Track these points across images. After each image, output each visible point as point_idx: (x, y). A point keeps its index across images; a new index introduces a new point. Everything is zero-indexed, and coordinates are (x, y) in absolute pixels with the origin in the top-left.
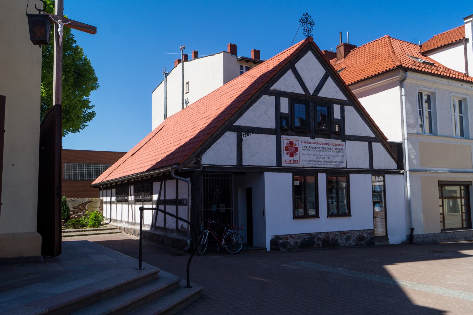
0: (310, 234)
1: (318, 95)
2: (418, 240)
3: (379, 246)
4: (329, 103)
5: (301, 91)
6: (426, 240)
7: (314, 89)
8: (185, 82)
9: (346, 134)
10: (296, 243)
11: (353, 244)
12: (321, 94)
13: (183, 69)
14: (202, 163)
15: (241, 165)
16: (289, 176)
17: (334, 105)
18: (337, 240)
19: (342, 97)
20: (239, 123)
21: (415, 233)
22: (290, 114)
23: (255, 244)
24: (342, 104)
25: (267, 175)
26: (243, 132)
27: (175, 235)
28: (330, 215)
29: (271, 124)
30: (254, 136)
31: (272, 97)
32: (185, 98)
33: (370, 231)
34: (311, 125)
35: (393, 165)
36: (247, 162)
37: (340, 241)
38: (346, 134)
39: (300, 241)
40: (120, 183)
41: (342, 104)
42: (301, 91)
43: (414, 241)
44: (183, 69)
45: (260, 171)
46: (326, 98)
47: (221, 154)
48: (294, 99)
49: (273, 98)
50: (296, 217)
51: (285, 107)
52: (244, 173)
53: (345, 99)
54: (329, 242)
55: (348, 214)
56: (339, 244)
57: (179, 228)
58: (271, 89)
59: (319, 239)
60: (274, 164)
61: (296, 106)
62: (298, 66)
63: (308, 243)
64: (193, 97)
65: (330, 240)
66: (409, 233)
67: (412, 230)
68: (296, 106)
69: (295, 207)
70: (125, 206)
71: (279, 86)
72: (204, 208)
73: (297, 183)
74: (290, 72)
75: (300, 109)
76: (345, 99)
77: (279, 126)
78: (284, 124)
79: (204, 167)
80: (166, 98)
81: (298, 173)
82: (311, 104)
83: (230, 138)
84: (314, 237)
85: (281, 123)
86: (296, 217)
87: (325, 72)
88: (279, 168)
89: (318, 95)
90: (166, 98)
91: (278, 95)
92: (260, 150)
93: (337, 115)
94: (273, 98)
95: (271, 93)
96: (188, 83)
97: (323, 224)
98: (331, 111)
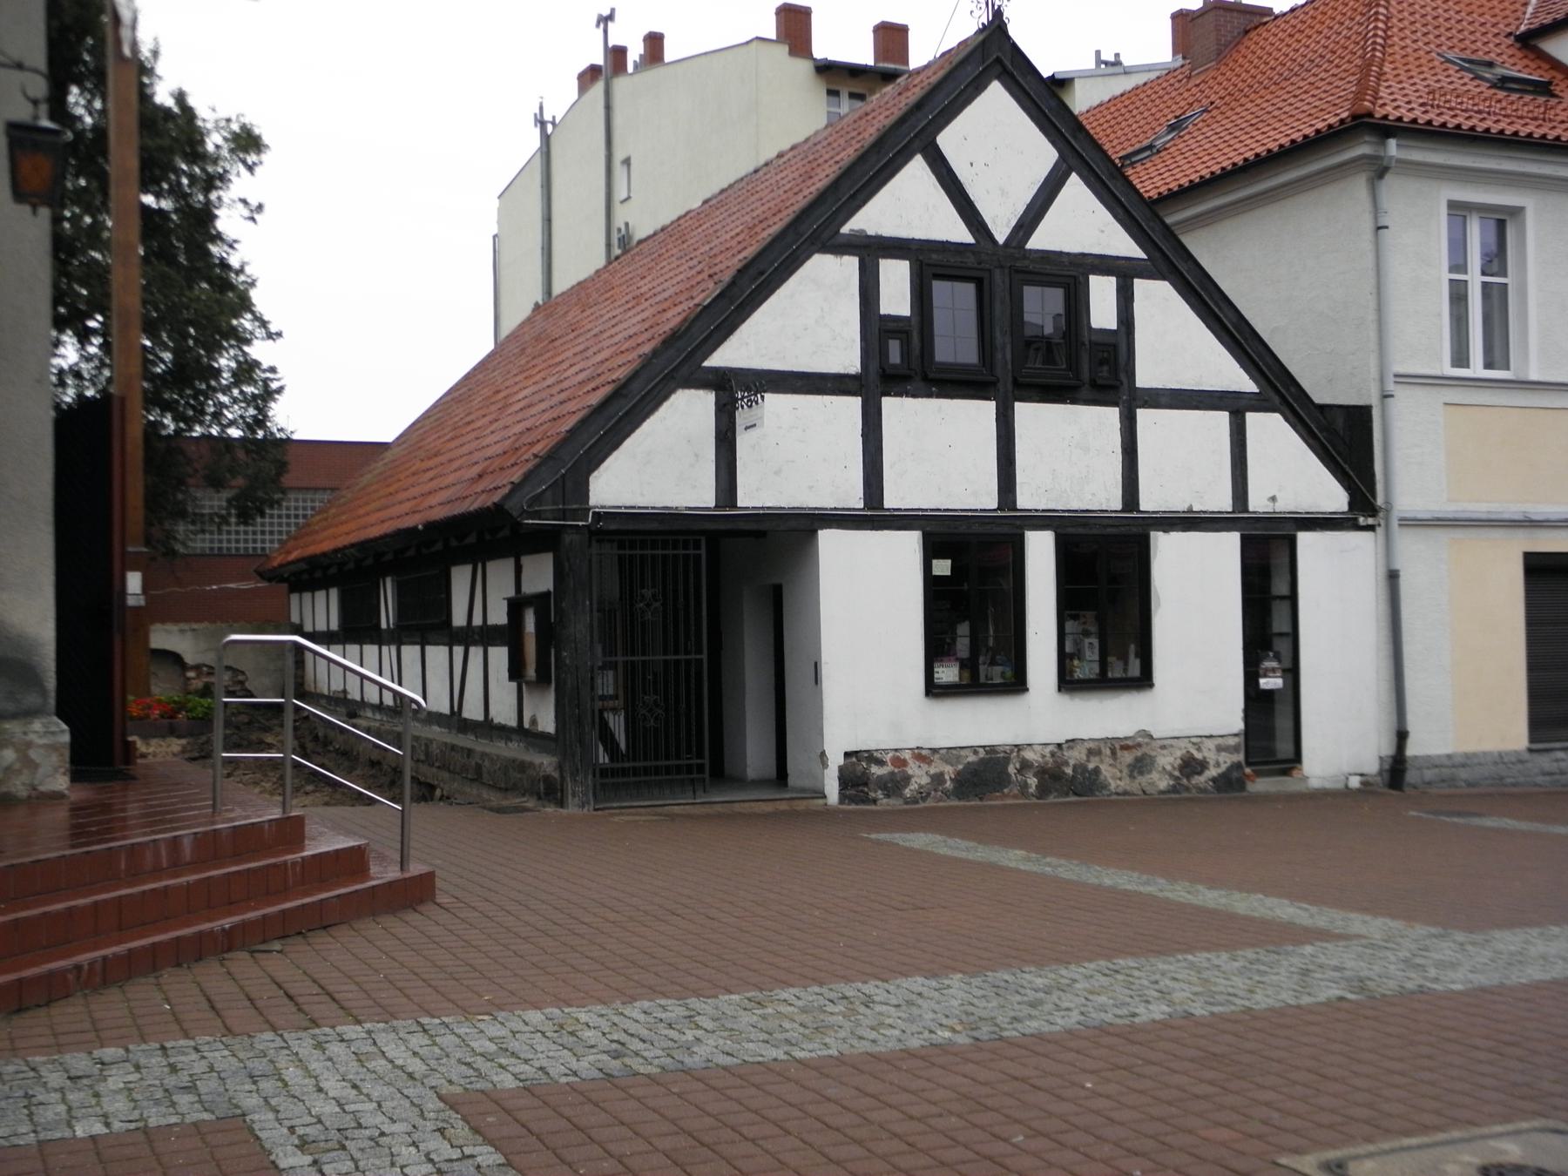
0: (991, 749)
1: (1029, 246)
2: (1429, 774)
3: (1266, 798)
4: (1070, 274)
5: (960, 233)
6: (1463, 774)
7: (1013, 223)
8: (619, 156)
9: (1139, 384)
10: (938, 779)
11: (1163, 784)
12: (1037, 242)
13: (608, 108)
14: (592, 502)
15: (734, 506)
16: (910, 543)
17: (1092, 278)
18: (1097, 771)
19: (1123, 245)
20: (721, 358)
21: (1412, 750)
22: (914, 322)
23: (792, 781)
24: (1124, 273)
25: (829, 541)
26: (735, 391)
27: (512, 750)
28: (1068, 682)
29: (847, 358)
30: (775, 404)
31: (846, 258)
32: (619, 222)
33: (1284, 748)
34: (999, 356)
35: (1332, 496)
36: (754, 494)
37: (1107, 772)
38: (1139, 384)
39: (949, 771)
40: (351, 566)
41: (1124, 273)
42: (960, 233)
43: (1411, 776)
44: (608, 108)
45: (794, 532)
46: (1061, 253)
47: (657, 468)
48: (930, 262)
49: (851, 264)
50: (934, 690)
51: (896, 297)
52: (761, 534)
53: (1137, 253)
54: (1066, 781)
55: (1144, 680)
56: (1105, 786)
57: (526, 725)
58: (845, 229)
59: (1025, 765)
60: (853, 498)
61: (940, 289)
62: (948, 140)
63: (984, 775)
64: (645, 216)
65: (1069, 771)
66: (1388, 749)
67: (1402, 736)
68: (940, 289)
69: (936, 649)
70: (437, 655)
71: (880, 215)
72: (604, 654)
73: (942, 567)
74: (916, 171)
75: (956, 301)
76: (1137, 253)
77: (874, 366)
78: (895, 356)
79: (598, 516)
80: (548, 220)
81: (943, 534)
82: (1000, 280)
83: (688, 413)
84: (1007, 760)
85: (884, 353)
86: (934, 690)
87: (1056, 155)
88: (874, 515)
89: (1029, 246)
90: (548, 220)
91: (872, 250)
92: (798, 456)
93: (1102, 310)
94: (851, 264)
95: (841, 247)
96: (627, 162)
97: (1042, 716)
98: (1077, 303)
